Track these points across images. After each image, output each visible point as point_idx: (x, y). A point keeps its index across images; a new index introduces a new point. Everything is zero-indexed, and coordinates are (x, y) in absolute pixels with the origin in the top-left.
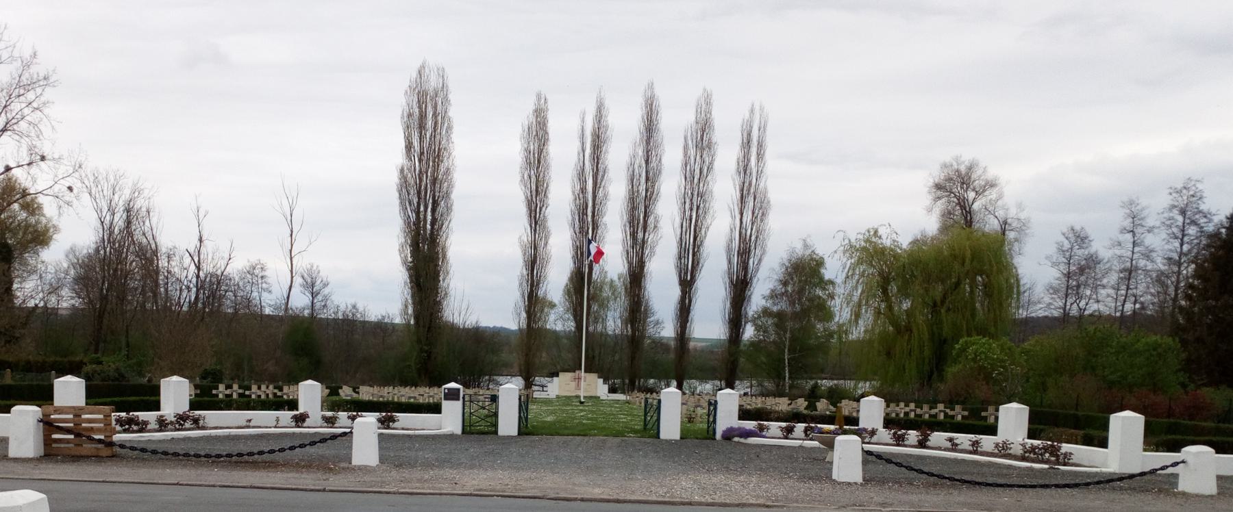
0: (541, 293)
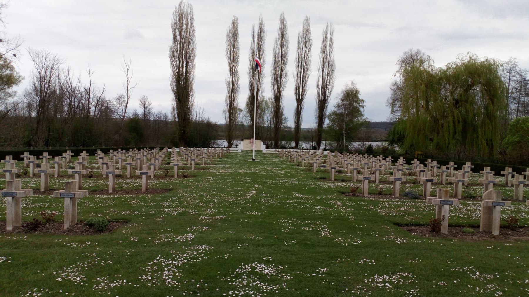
0: (235, 105)
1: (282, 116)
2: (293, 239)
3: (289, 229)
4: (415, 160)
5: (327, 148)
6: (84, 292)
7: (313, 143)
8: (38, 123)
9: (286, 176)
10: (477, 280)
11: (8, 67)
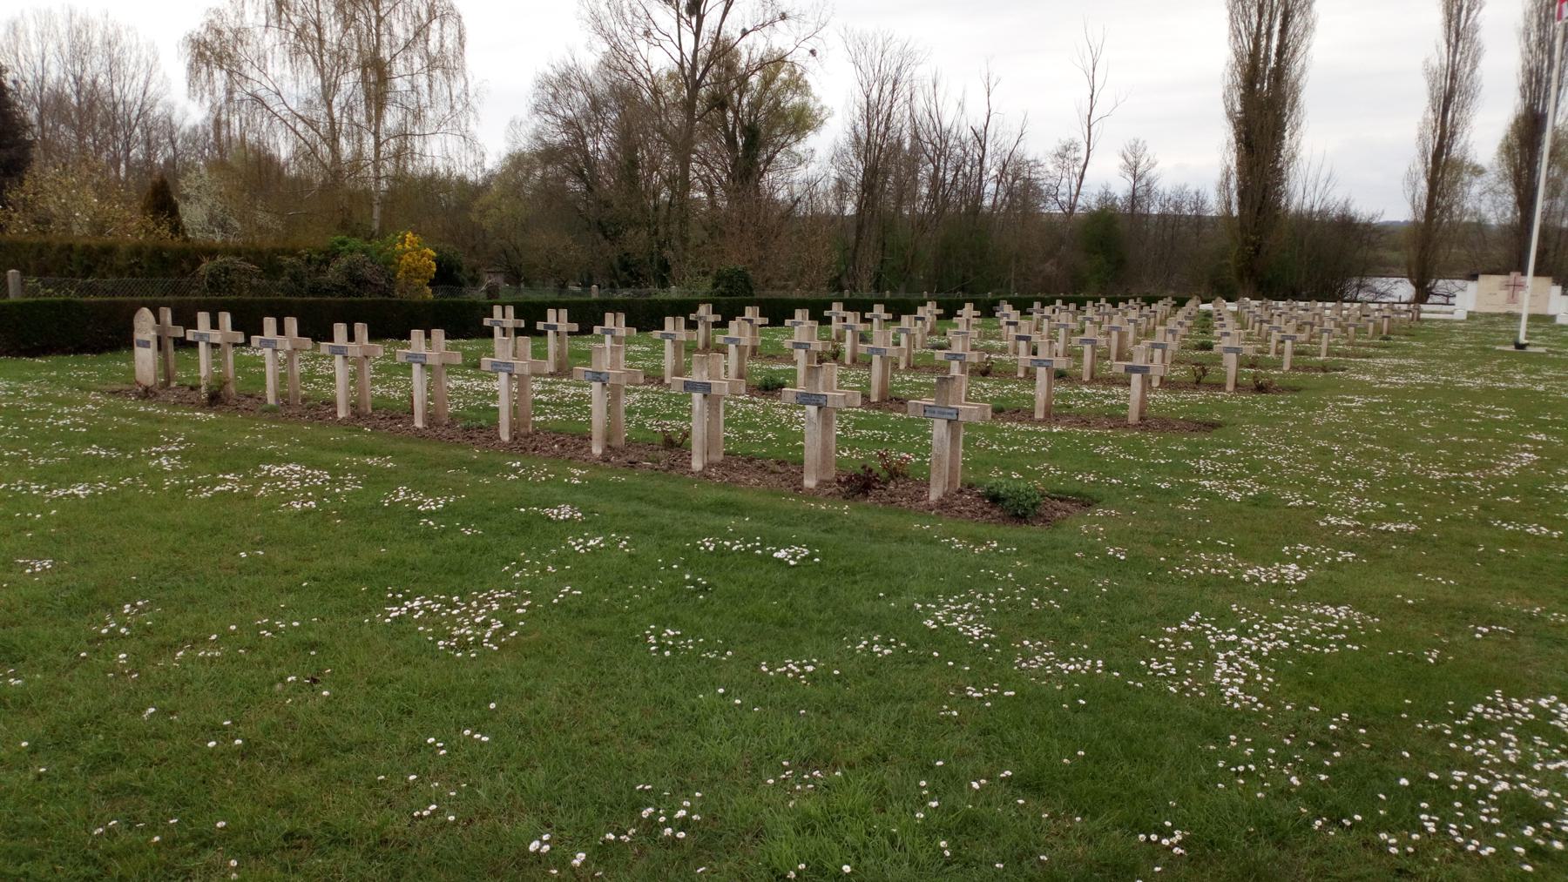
0: (1455, 152)
6: (991, 668)
8: (860, 228)
11: (798, 87)
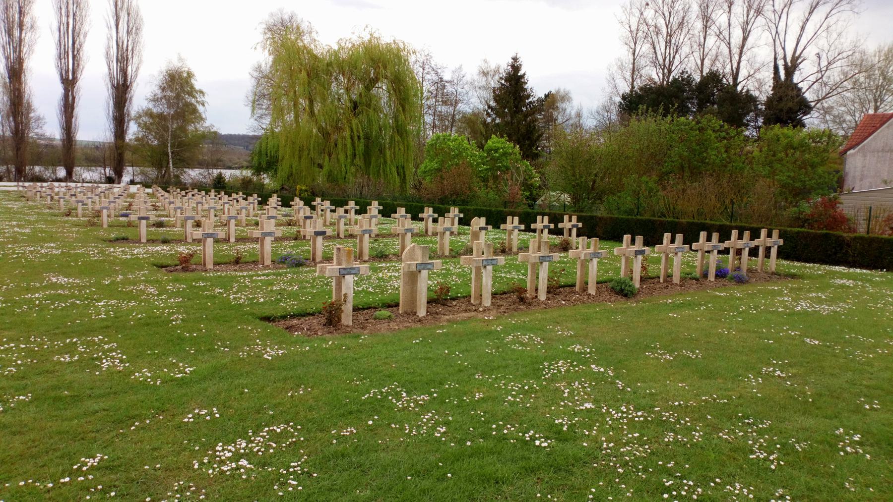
1: (28, 113)
2: (23, 390)
3: (17, 366)
4: (297, 199)
5: (137, 179)
7: (107, 170)
9: (35, 239)
10: (404, 409)
